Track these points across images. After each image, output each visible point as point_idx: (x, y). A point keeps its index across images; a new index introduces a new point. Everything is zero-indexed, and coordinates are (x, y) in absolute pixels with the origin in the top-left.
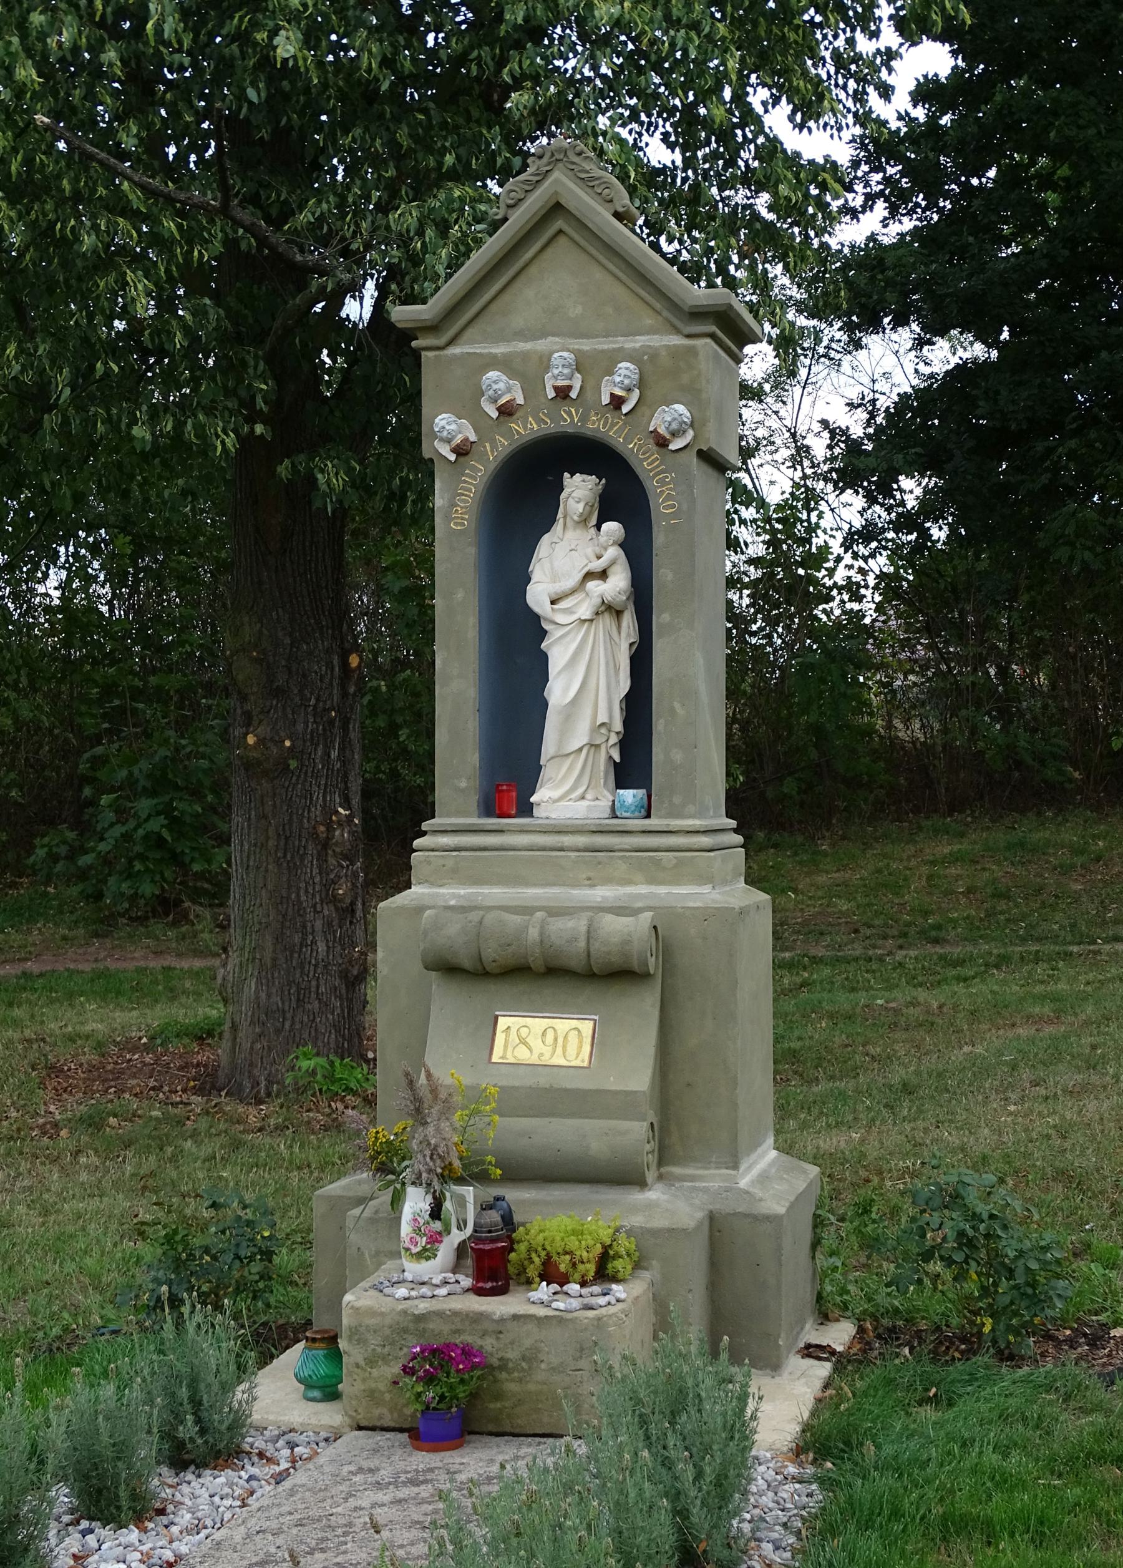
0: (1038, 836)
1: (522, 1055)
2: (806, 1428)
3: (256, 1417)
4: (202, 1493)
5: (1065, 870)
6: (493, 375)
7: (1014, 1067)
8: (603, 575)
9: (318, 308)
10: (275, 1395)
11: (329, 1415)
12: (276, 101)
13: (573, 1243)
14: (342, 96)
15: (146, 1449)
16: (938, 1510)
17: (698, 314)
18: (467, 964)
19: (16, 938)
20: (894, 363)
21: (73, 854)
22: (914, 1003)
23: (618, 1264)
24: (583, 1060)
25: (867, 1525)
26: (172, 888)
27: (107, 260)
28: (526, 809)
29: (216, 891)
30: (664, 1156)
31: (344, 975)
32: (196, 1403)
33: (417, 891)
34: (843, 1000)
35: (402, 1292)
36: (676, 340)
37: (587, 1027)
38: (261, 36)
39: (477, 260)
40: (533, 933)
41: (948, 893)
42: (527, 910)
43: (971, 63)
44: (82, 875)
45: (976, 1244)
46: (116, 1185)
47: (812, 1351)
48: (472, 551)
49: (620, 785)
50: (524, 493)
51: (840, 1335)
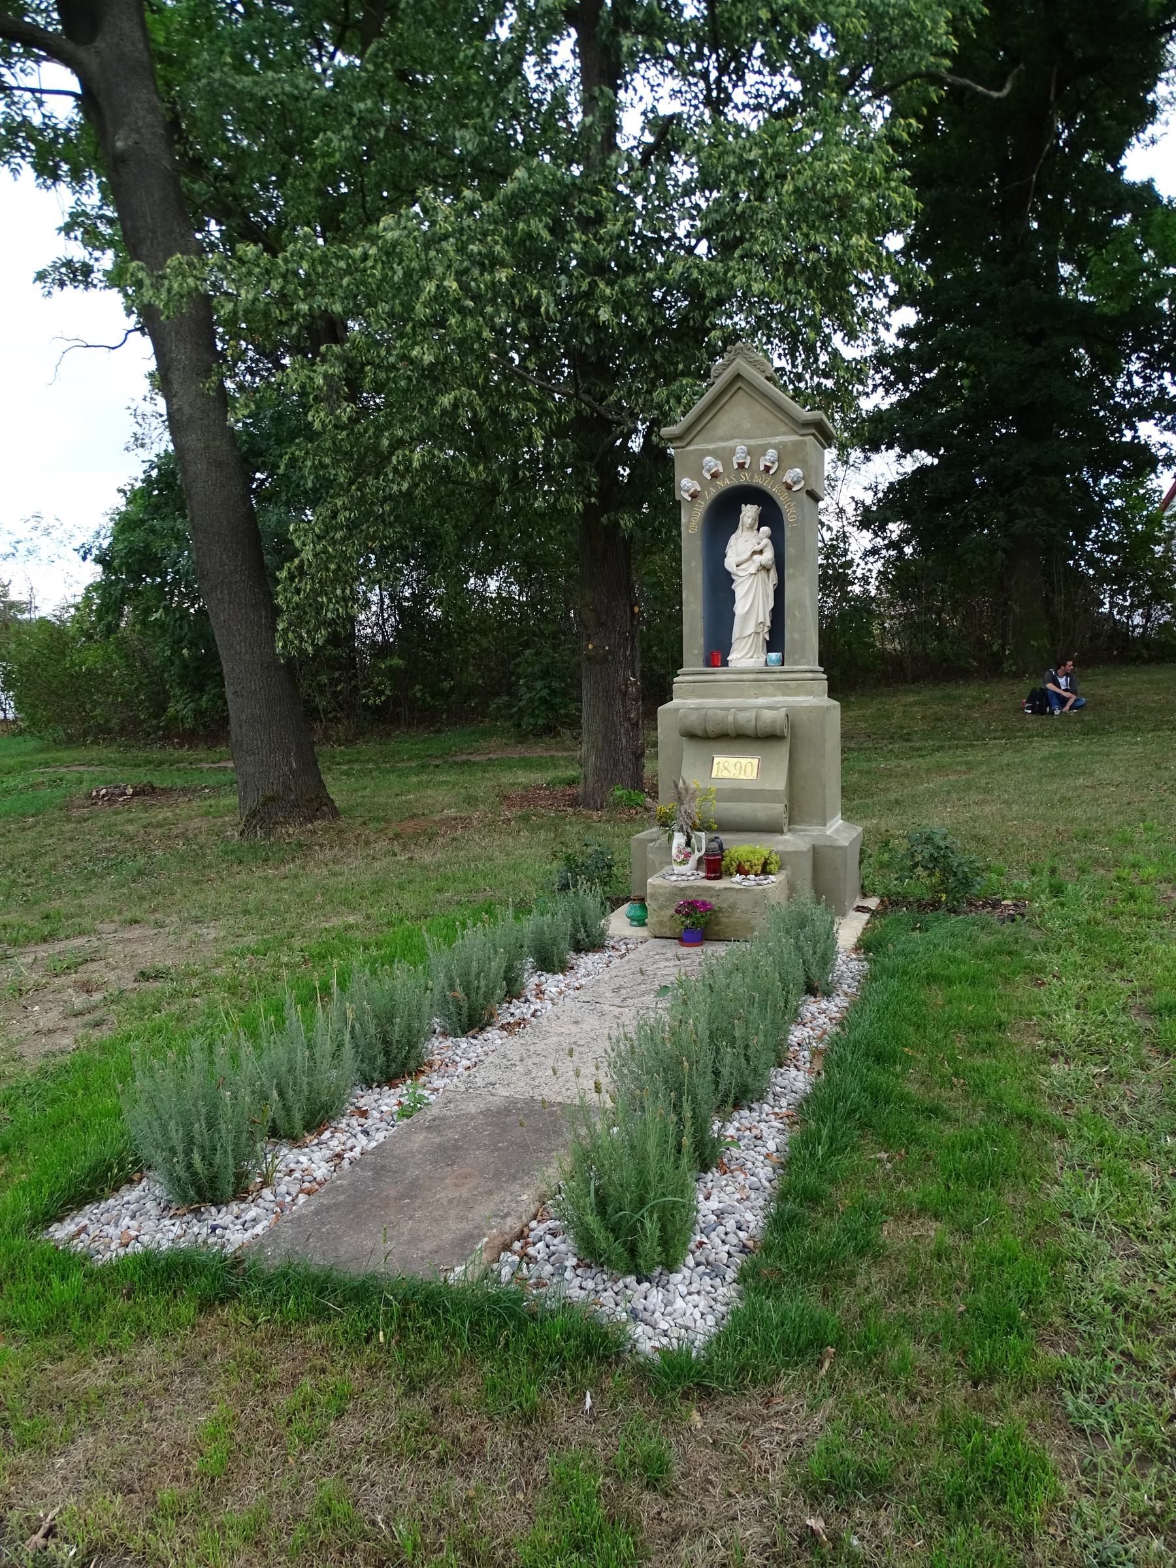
0: (956, 692)
1: (726, 775)
2: (859, 940)
3: (610, 932)
4: (588, 962)
5: (970, 708)
6: (708, 458)
7: (949, 792)
8: (761, 552)
9: (618, 443)
10: (618, 923)
11: (642, 932)
12: (599, 343)
13: (751, 857)
14: (629, 340)
15: (564, 945)
16: (924, 972)
17: (806, 424)
18: (700, 733)
19: (485, 744)
20: (888, 467)
21: (509, 706)
22: (899, 766)
23: (772, 867)
24: (754, 776)
25: (893, 976)
26: (552, 721)
27: (522, 423)
28: (725, 663)
29: (574, 723)
30: (791, 821)
31: (634, 753)
32: (585, 925)
33: (675, 702)
34: (865, 766)
35: (674, 878)
36: (796, 438)
37: (755, 761)
38: (592, 311)
39: (700, 404)
40: (730, 718)
41: (913, 719)
42: (728, 709)
43: (926, 317)
44: (511, 716)
45: (938, 860)
46: (538, 844)
47: (859, 909)
48: (699, 543)
49: (769, 651)
50: (723, 515)
51: (873, 903)
